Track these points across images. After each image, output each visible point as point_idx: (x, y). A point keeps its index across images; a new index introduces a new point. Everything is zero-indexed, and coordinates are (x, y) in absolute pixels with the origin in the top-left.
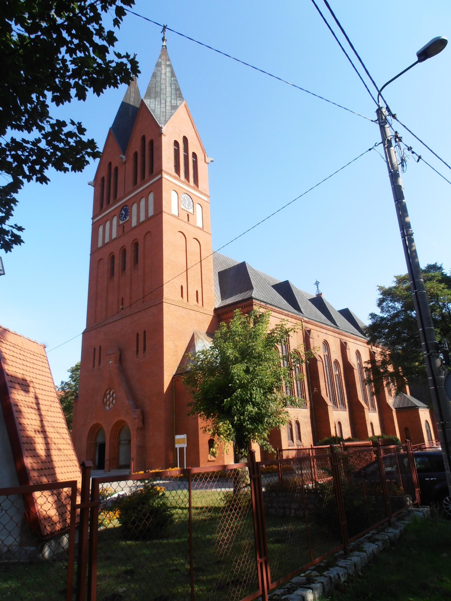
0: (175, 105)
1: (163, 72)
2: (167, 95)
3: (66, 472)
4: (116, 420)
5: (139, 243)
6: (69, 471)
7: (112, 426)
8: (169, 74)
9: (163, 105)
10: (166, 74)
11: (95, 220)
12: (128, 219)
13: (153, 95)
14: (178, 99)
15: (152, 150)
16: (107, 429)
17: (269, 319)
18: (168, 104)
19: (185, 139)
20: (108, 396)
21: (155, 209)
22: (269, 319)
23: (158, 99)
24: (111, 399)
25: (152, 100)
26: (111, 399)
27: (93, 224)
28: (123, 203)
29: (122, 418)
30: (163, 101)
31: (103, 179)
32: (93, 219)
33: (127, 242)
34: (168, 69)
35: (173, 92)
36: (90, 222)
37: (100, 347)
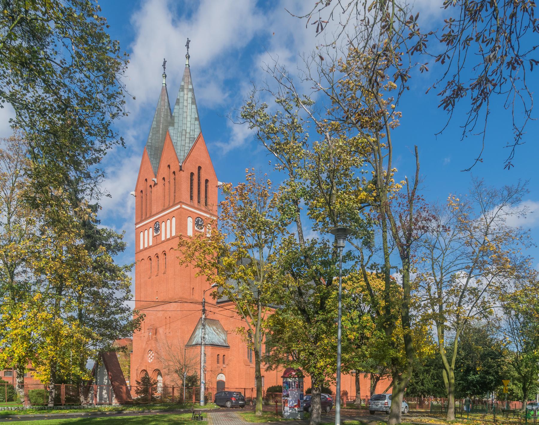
1: (185, 98)
9: (183, 138)
10: (187, 100)
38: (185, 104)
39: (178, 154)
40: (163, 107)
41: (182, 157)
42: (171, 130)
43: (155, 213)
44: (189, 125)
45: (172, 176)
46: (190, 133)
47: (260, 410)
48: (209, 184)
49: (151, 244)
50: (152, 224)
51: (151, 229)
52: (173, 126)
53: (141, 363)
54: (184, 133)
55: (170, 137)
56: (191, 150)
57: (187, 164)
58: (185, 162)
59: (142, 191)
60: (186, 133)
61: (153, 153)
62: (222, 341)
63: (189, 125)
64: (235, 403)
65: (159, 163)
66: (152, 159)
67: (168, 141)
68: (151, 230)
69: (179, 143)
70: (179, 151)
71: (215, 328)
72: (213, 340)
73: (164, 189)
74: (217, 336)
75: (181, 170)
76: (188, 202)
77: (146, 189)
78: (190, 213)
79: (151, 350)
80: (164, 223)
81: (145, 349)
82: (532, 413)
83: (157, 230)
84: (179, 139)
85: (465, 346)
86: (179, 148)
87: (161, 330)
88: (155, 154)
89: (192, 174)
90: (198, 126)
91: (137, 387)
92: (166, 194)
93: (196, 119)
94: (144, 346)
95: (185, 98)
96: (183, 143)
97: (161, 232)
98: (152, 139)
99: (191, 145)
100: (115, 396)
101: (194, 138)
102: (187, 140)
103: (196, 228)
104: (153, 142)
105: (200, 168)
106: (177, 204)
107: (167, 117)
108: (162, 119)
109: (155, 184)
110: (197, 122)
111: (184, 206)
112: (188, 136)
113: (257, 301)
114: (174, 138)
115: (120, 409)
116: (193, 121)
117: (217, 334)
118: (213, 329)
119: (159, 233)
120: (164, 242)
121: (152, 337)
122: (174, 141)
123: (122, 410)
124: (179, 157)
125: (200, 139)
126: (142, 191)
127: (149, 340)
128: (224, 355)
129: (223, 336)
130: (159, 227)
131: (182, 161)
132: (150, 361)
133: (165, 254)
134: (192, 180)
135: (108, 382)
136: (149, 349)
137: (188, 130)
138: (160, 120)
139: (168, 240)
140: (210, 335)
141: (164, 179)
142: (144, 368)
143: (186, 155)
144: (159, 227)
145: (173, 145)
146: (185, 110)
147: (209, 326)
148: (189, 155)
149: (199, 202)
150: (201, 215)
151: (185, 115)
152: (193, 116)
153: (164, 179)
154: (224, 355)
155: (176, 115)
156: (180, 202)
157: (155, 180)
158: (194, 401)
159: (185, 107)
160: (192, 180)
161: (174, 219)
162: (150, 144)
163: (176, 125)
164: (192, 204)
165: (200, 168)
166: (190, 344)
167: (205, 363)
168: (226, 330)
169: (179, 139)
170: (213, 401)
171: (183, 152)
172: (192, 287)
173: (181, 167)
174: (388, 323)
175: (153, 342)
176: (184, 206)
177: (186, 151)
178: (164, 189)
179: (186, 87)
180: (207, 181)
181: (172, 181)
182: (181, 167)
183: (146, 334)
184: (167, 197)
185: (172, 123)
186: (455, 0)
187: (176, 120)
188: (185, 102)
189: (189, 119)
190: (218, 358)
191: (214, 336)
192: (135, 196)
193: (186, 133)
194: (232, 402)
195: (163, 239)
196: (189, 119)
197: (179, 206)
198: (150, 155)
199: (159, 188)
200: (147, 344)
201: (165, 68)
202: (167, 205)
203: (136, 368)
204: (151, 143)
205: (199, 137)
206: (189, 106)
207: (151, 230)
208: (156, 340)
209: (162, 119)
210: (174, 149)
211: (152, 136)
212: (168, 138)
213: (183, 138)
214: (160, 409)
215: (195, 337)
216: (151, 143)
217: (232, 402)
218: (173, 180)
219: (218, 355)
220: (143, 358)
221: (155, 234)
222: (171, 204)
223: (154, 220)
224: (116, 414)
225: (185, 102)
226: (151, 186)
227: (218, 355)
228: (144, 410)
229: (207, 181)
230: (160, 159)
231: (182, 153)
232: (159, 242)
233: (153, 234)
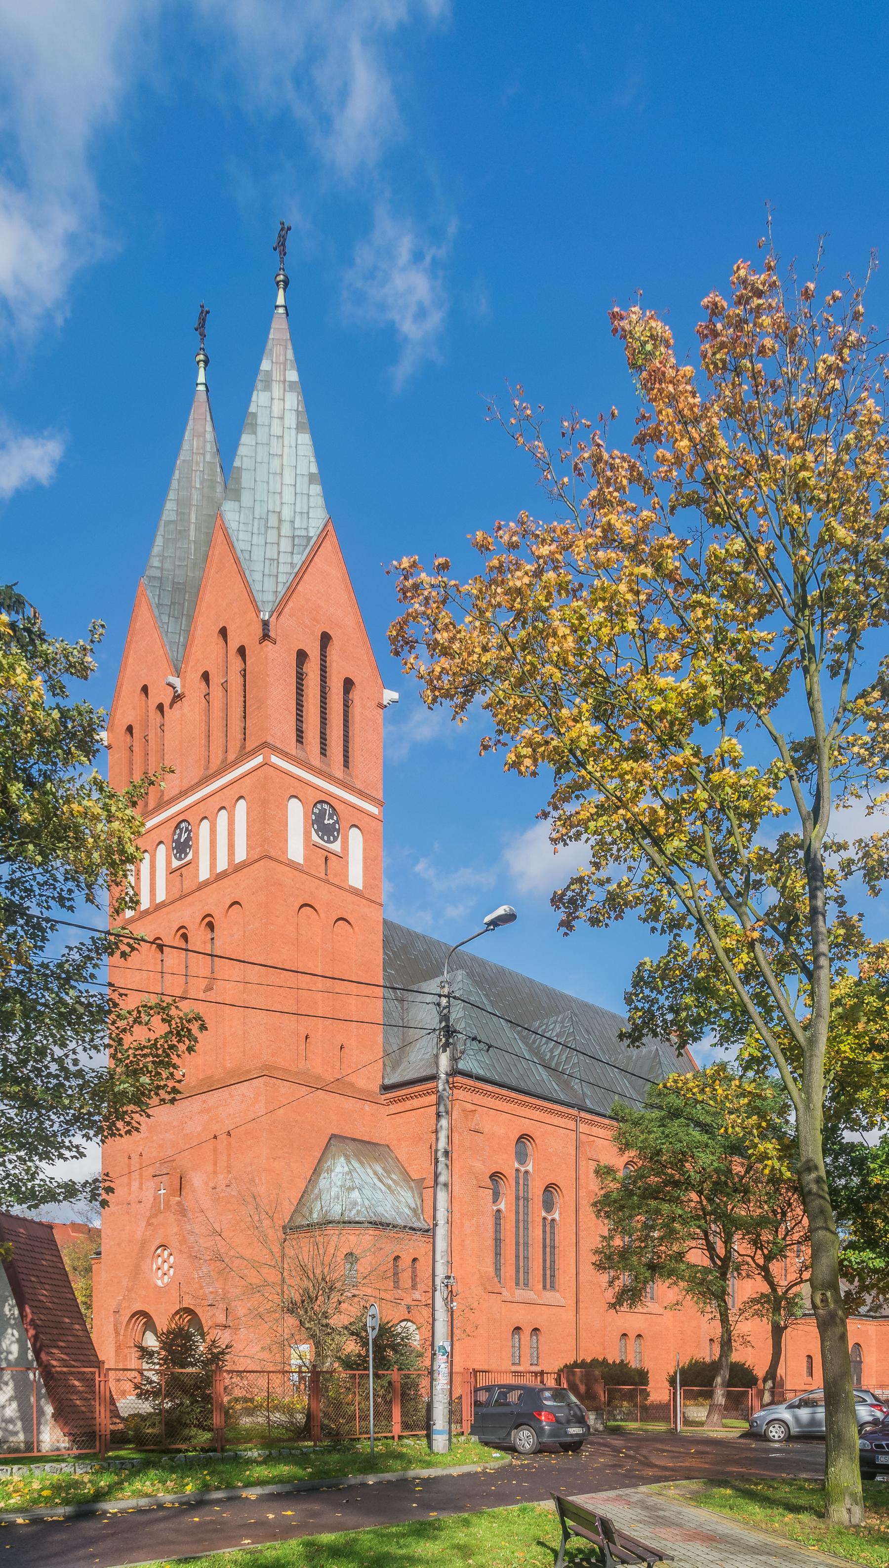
0: (303, 533)
9: (272, 536)
10: (282, 418)
38: (276, 430)
39: (256, 587)
40: (199, 458)
41: (269, 597)
42: (230, 513)
43: (176, 791)
44: (288, 497)
45: (236, 664)
46: (293, 522)
47: (853, 1495)
48: (356, 695)
49: (161, 896)
50: (166, 832)
51: (162, 849)
52: (237, 498)
53: (129, 1290)
54: (273, 521)
55: (227, 536)
56: (300, 575)
58: (279, 609)
59: (130, 729)
60: (280, 521)
61: (167, 602)
62: (407, 1210)
63: (288, 497)
64: (553, 1434)
65: (185, 646)
66: (165, 619)
67: (219, 549)
68: (162, 850)
69: (258, 554)
70: (258, 576)
71: (380, 1170)
72: (380, 1209)
73: (208, 711)
74: (390, 1197)
75: (266, 636)
76: (291, 746)
77: (145, 724)
78: (297, 783)
79: (164, 1246)
80: (205, 824)
81: (144, 1244)
83: (181, 847)
84: (258, 540)
86: (258, 567)
87: (197, 1180)
88: (173, 603)
89: (302, 656)
90: (320, 501)
91: (140, 1372)
92: (213, 724)
93: (312, 478)
94: (139, 1235)
95: (276, 411)
96: (272, 552)
97: (196, 854)
98: (163, 558)
99: (298, 559)
100: (49, 1410)
101: (309, 538)
102: (285, 545)
103: (315, 838)
104: (168, 565)
105: (326, 639)
106: (254, 753)
107: (212, 488)
108: (195, 496)
109: (177, 698)
110: (316, 489)
111: (275, 760)
112: (286, 530)
114: (242, 536)
115: (89, 1490)
116: (303, 484)
117: (389, 1187)
118: (375, 1173)
119: (190, 857)
120: (206, 884)
121: (167, 1203)
122: (240, 546)
123: (100, 1496)
124: (259, 597)
125: (327, 544)
126: (130, 729)
127: (156, 1212)
128: (415, 1260)
129: (407, 1198)
130: (189, 838)
131: (269, 608)
132: (159, 1283)
133: (211, 926)
134: (300, 677)
135: (23, 1351)
136: (157, 1243)
137: (287, 514)
138: (190, 498)
139: (224, 875)
140: (367, 1192)
141: (206, 676)
142: (138, 1307)
143: (282, 589)
144: (189, 838)
145: (237, 560)
146: (275, 448)
147: (361, 1163)
148: (291, 590)
149: (323, 752)
150: (331, 795)
151: (275, 464)
152: (303, 469)
153: (206, 676)
154: (415, 1260)
155: (247, 464)
156: (264, 745)
157: (177, 682)
158: (397, 1429)
159: (274, 441)
160: (300, 677)
161: (242, 805)
162: (157, 573)
163: (246, 497)
164: (301, 754)
165: (326, 639)
166: (300, 1221)
167: (450, 1264)
168: (415, 1176)
169: (258, 540)
170: (467, 1427)
171: (273, 580)
172: (303, 1033)
173: (265, 624)
175: (172, 1218)
176: (275, 760)
177: (282, 578)
178: (208, 711)
179: (276, 376)
180: (348, 684)
181: (235, 681)
182: (265, 624)
183: (148, 1195)
184: (217, 734)
185: (232, 488)
187: (246, 480)
188: (276, 422)
189: (288, 478)
190: (544, 1226)
191: (379, 1195)
193: (280, 521)
194: (539, 1432)
195: (204, 874)
196: (288, 478)
197: (259, 760)
198: (159, 605)
199: (191, 708)
200: (149, 1224)
202: (216, 763)
203: (114, 1306)
204: (161, 569)
205: (323, 536)
206: (290, 437)
207: (162, 850)
208: (182, 1211)
209: (195, 496)
210: (241, 572)
211: (164, 548)
212: (220, 537)
213: (272, 536)
214: (278, 1480)
216: (162, 569)
217: (539, 1432)
218: (240, 680)
219: (397, 1258)
220: (136, 1271)
221: (176, 863)
222: (231, 757)
223: (172, 818)
224: (68, 1518)
225: (276, 422)
226: (160, 707)
227: (397, 1258)
228: (206, 1488)
229: (348, 684)
230: (191, 618)
231: (269, 585)
232: (188, 885)
233: (169, 862)
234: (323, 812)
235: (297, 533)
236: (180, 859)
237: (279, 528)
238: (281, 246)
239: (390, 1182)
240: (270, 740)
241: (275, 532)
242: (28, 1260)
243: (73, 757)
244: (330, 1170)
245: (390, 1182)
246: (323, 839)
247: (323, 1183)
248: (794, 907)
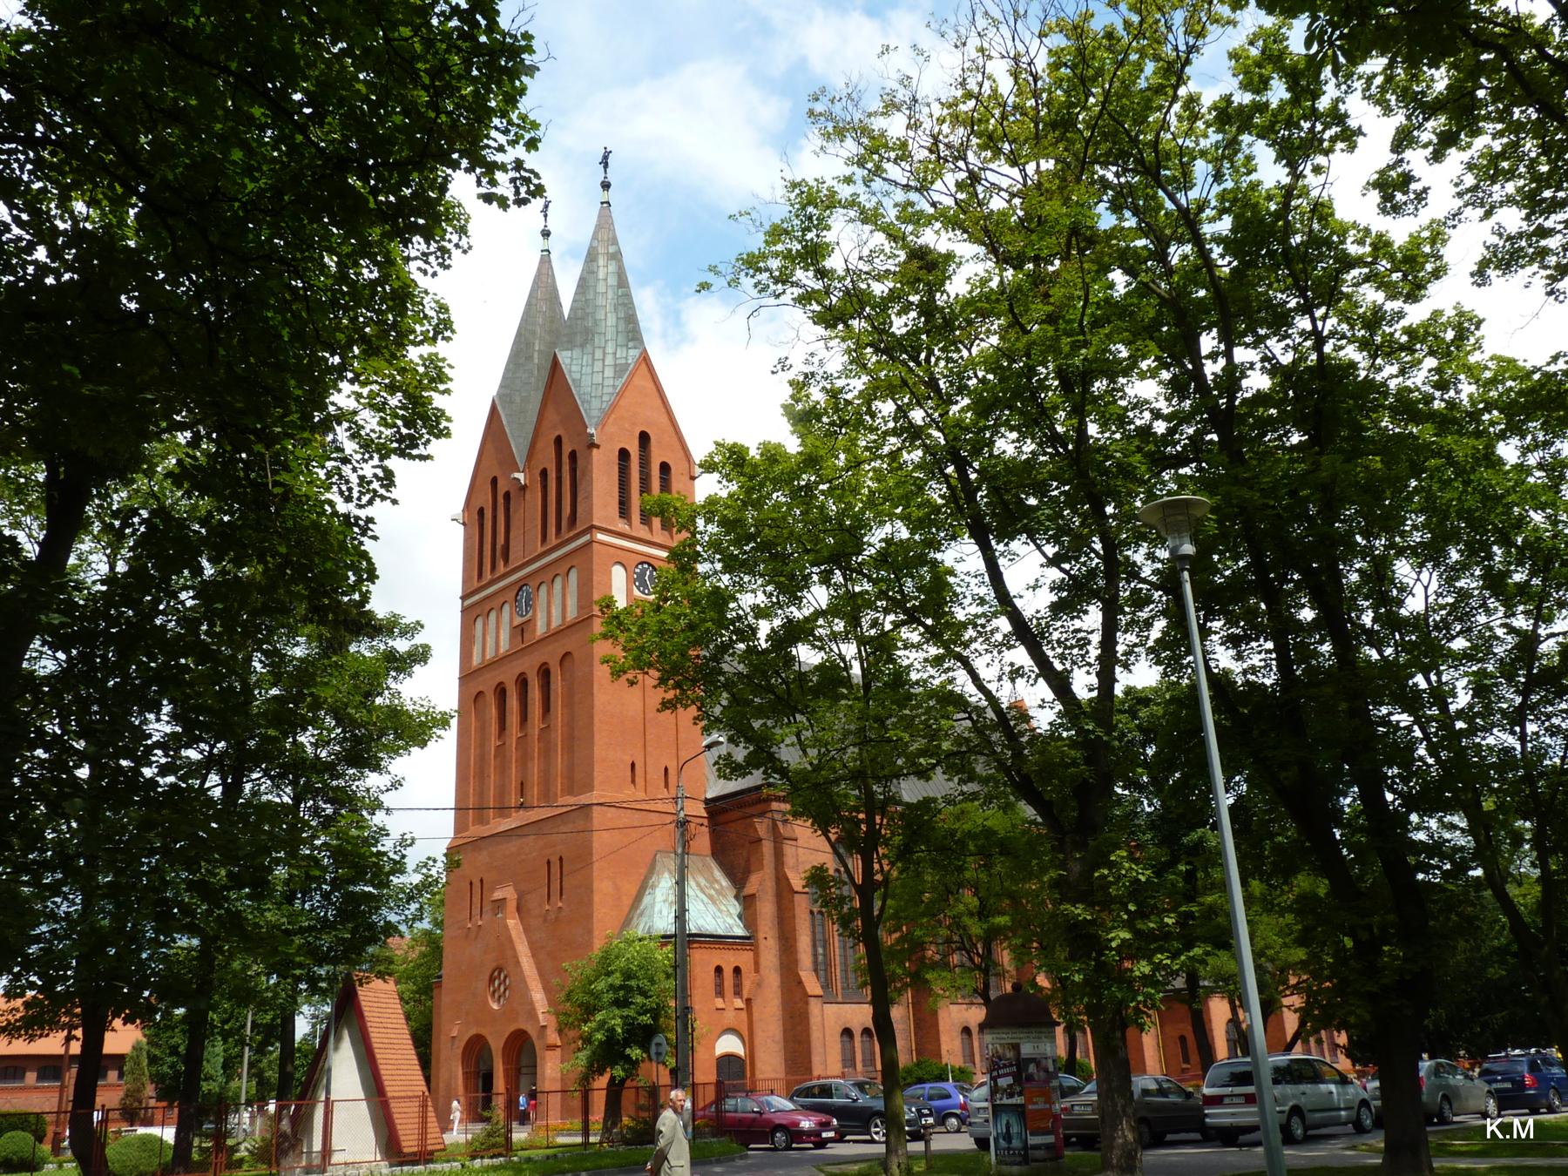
0: (623, 361)
1: (601, 275)
2: (609, 337)
3: (604, 196)
4: (512, 1028)
5: (552, 670)
6: (612, 195)
7: (504, 1040)
8: (612, 281)
9: (598, 366)
10: (606, 280)
11: (468, 602)
12: (530, 614)
13: (579, 339)
14: (631, 344)
15: (573, 471)
16: (496, 1044)
17: (1254, 177)
18: (609, 360)
19: (644, 438)
20: (497, 983)
21: (580, 608)
22: (1254, 177)
23: (589, 347)
24: (502, 989)
25: (577, 353)
26: (502, 989)
27: (464, 611)
28: (521, 580)
29: (523, 1026)
30: (599, 354)
31: (481, 512)
32: (463, 598)
33: (529, 665)
34: (612, 267)
35: (622, 324)
36: (457, 605)
37: (482, 881)
41: (595, 413)
56: (621, 394)
57: (610, 428)
71: (703, 882)
78: (619, 552)
82: (1004, 1082)
85: (828, 245)
89: (624, 454)
99: (620, 383)
102: (609, 372)
103: (636, 593)
112: (609, 360)
113: (10, 509)
114: (574, 368)
148: (614, 407)
171: (598, 400)
174: (1115, 734)
186: (1567, 38)
192: (464, 524)
195: (540, 629)
201: (546, 216)
215: (641, 914)
221: (518, 620)
225: (602, 283)
234: (644, 571)
235: (618, 362)
236: (522, 616)
237: (603, 360)
238: (605, 162)
239: (713, 892)
240: (596, 523)
241: (600, 363)
242: (535, 769)
243: (975, 991)
244: (653, 887)
245: (713, 892)
246: (643, 593)
247: (646, 900)
248: (1234, 648)
